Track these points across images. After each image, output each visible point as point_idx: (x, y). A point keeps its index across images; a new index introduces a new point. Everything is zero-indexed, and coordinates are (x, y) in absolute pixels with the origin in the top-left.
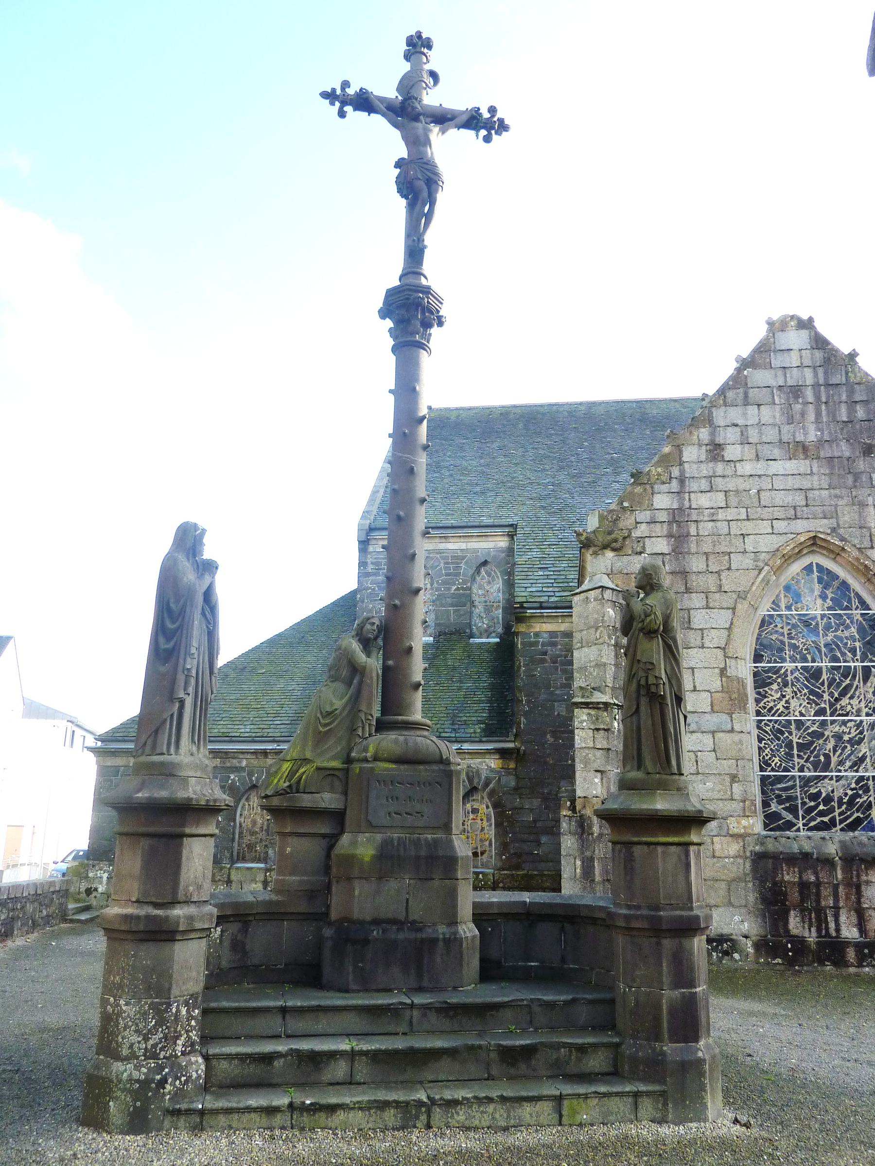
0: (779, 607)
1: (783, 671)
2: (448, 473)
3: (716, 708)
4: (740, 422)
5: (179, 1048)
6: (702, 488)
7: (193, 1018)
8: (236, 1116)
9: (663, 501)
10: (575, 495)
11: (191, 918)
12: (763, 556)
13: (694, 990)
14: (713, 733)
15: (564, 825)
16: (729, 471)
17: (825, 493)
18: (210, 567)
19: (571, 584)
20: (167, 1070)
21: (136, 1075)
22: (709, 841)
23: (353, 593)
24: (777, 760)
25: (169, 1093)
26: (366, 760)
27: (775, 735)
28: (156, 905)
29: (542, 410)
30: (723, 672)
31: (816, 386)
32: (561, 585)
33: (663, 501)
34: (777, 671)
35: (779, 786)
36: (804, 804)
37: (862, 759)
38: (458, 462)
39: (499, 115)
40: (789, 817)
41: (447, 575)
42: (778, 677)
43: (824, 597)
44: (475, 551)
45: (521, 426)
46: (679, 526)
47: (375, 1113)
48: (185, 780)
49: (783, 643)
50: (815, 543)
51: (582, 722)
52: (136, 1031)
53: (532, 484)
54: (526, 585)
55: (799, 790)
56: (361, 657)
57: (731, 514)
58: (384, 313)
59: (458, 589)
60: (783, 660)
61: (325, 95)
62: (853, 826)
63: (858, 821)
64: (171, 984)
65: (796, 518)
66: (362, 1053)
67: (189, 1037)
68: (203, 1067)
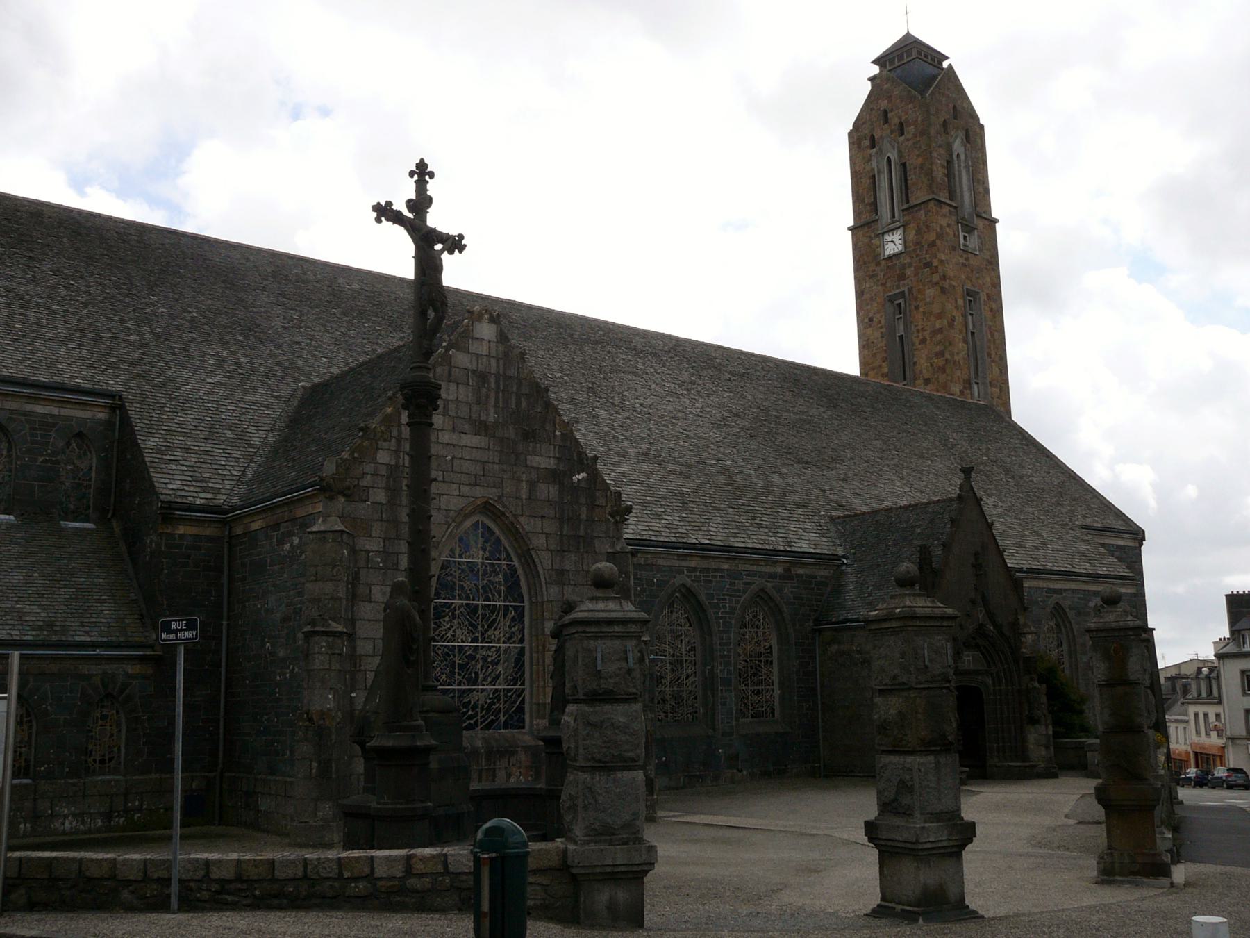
12: (452, 514)
17: (496, 467)
29: (79, 218)
31: (497, 376)
34: (448, 606)
37: (498, 676)
43: (484, 549)
50: (487, 508)
59: (45, 461)
62: (488, 727)
63: (492, 722)
65: (476, 485)
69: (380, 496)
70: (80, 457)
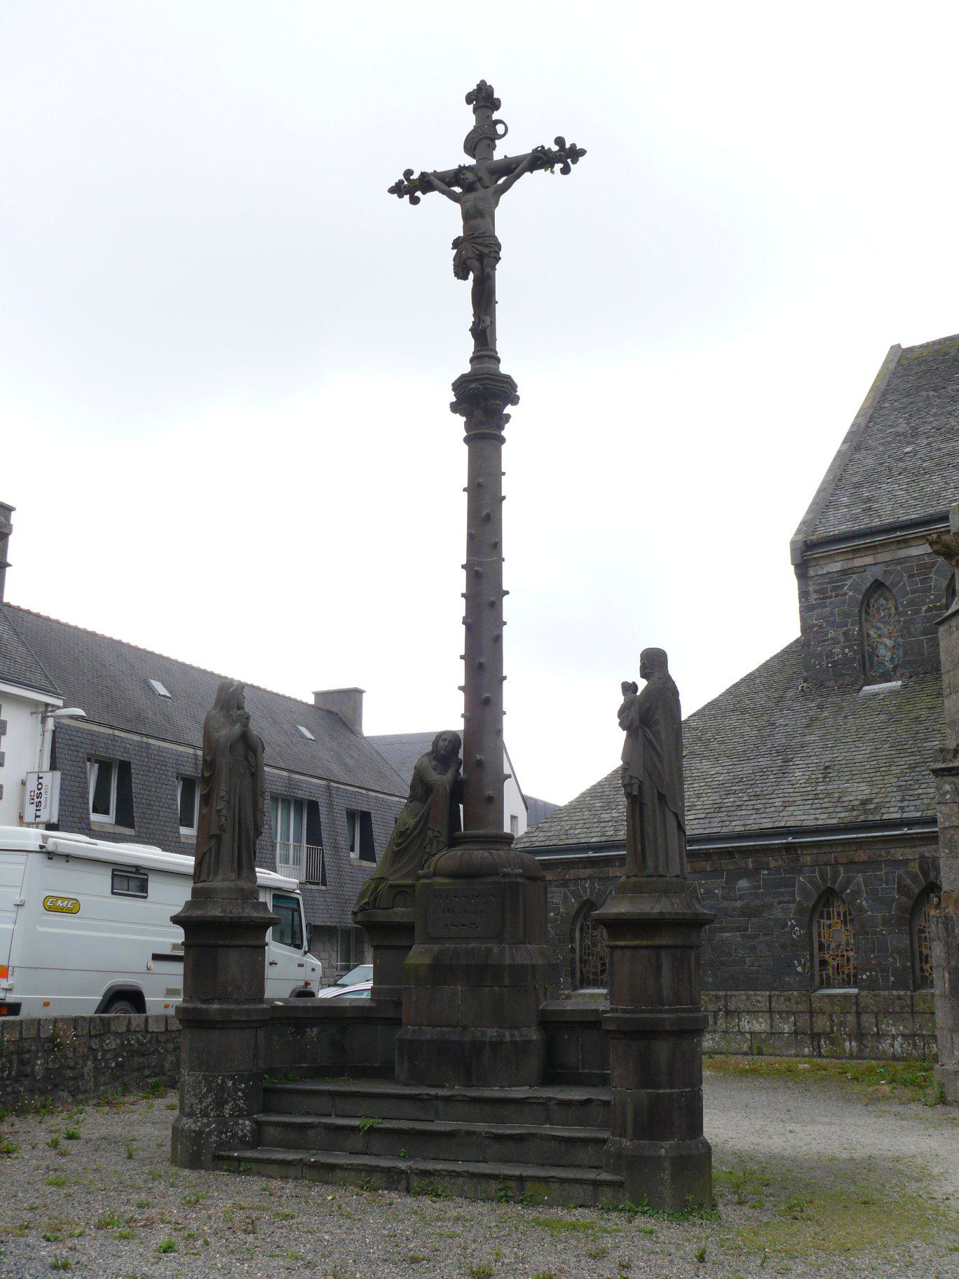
21: (193, 1127)
41: (913, 592)
52: (195, 1095)
59: (930, 609)
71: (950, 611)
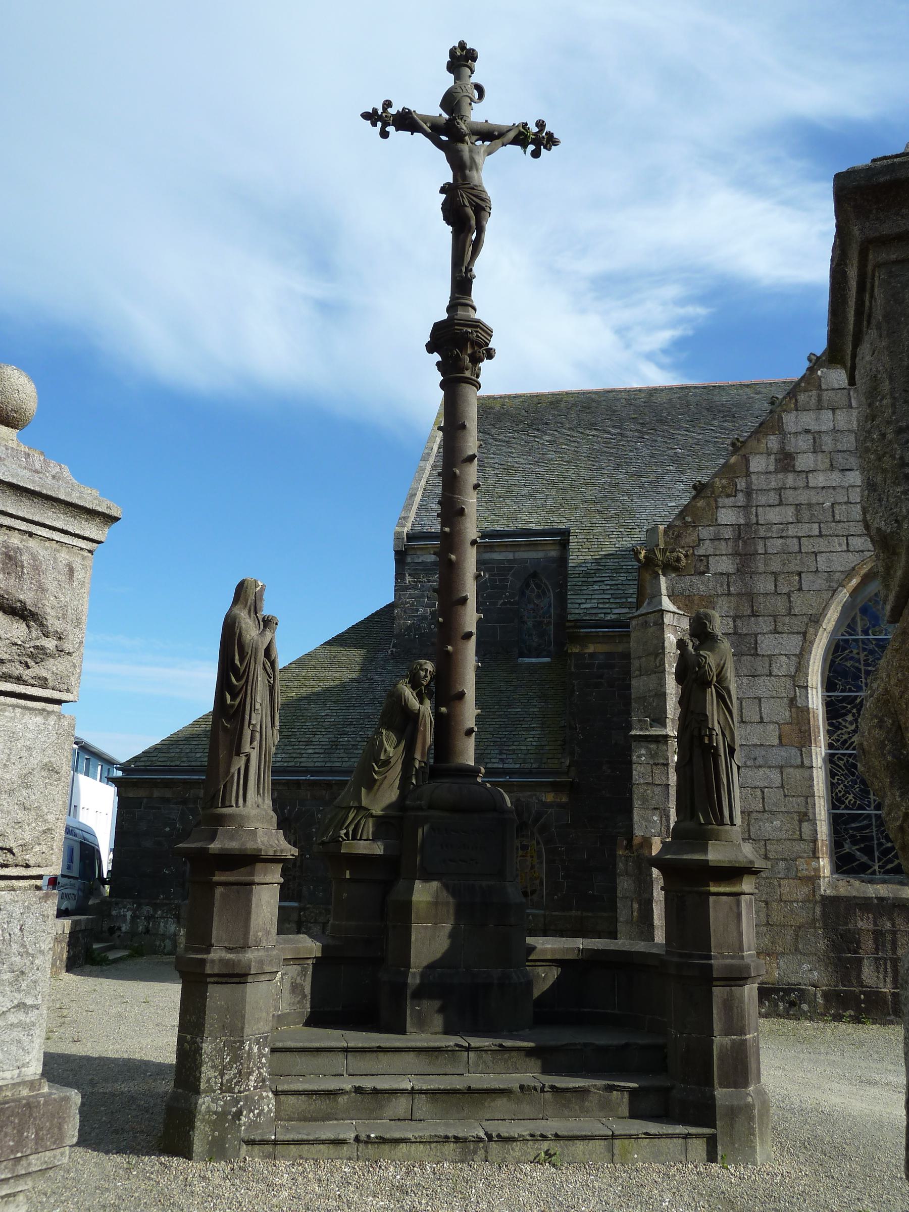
0: (854, 630)
1: (858, 700)
2: (492, 472)
3: (784, 741)
4: (814, 427)
5: (252, 1083)
6: (771, 502)
7: (264, 1055)
8: (306, 1147)
9: (727, 516)
10: (635, 497)
11: (261, 962)
13: (743, 1037)
14: (781, 768)
15: (621, 866)
16: (801, 483)
18: (268, 623)
19: (630, 600)
20: (241, 1103)
21: (214, 1107)
22: (776, 883)
23: (390, 607)
24: (851, 797)
25: (245, 1123)
26: (420, 808)
27: (849, 770)
28: (229, 950)
30: (792, 701)
32: (618, 601)
33: (727, 516)
35: (853, 825)
36: (880, 844)
38: (504, 460)
39: (547, 129)
40: (864, 859)
41: (493, 587)
42: (853, 707)
44: (524, 561)
45: (573, 416)
46: (745, 542)
47: (436, 1147)
48: (254, 833)
49: (859, 670)
51: (639, 757)
52: (212, 1067)
53: (586, 484)
54: (579, 601)
55: (874, 829)
56: (414, 703)
57: (803, 529)
58: (431, 348)
59: (504, 603)
60: (859, 689)
61: (366, 116)
64: (244, 1023)
66: (421, 1092)
67: (260, 1073)
68: (273, 1101)
69: (724, 565)
70: (539, 596)
71: (639, 612)
